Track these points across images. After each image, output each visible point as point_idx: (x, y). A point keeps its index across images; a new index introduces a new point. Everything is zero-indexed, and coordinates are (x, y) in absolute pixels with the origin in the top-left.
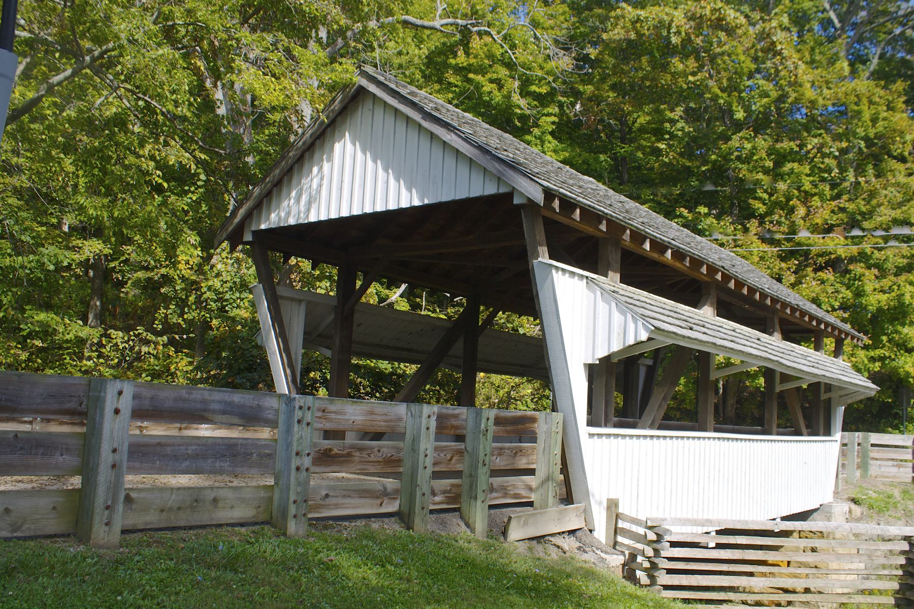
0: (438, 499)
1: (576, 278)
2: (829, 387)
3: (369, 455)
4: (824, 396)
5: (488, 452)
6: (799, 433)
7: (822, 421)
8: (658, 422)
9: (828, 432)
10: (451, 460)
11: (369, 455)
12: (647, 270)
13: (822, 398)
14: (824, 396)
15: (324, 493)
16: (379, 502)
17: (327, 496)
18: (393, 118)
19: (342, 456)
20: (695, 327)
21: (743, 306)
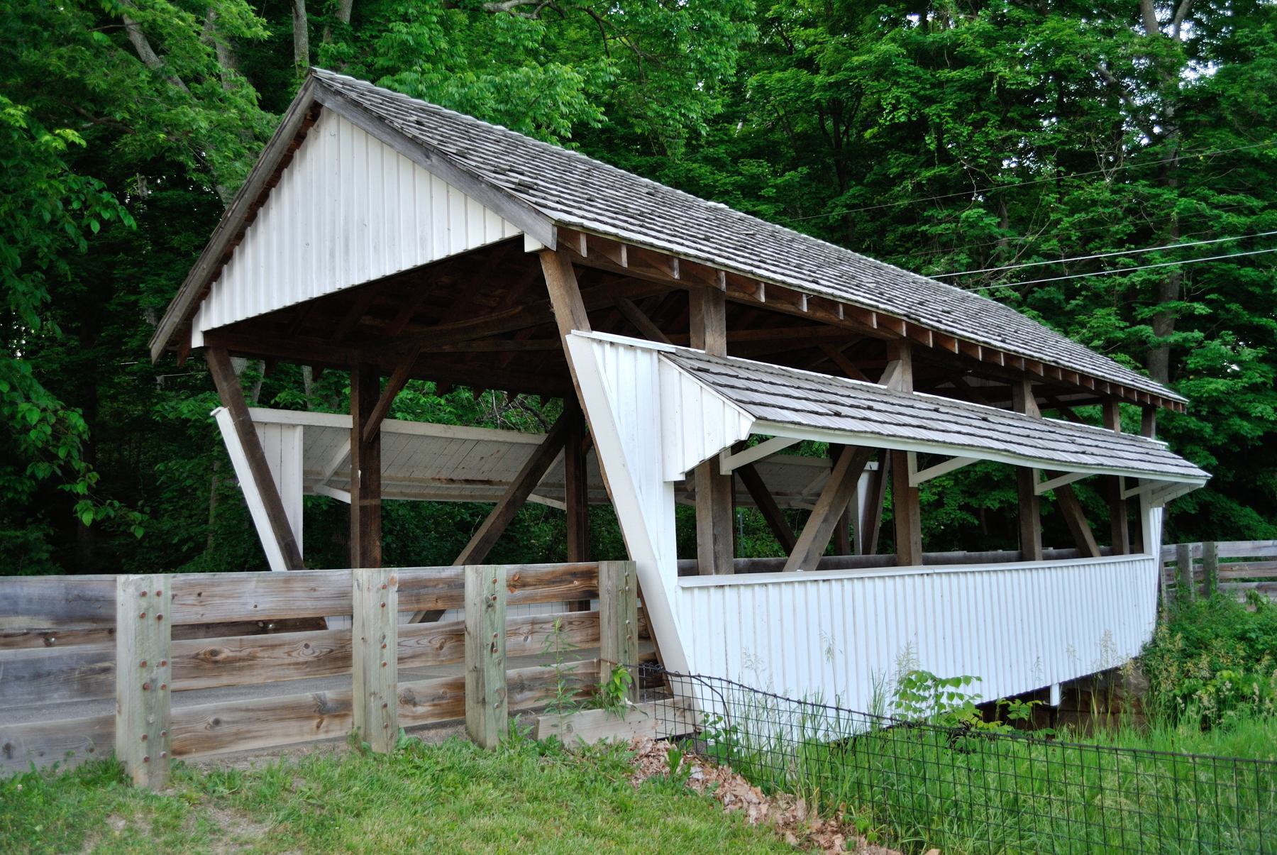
0: (420, 710)
1: (900, 376)
2: (1132, 482)
3: (289, 654)
4: (1125, 495)
5: (499, 631)
6: (1086, 553)
7: (1125, 531)
8: (817, 558)
9: (1137, 545)
10: (441, 648)
11: (289, 654)
12: (775, 331)
13: (1123, 498)
14: (1125, 495)
15: (211, 720)
16: (315, 722)
17: (217, 722)
18: (395, 164)
19: (240, 659)
20: (942, 409)
21: (953, 370)
